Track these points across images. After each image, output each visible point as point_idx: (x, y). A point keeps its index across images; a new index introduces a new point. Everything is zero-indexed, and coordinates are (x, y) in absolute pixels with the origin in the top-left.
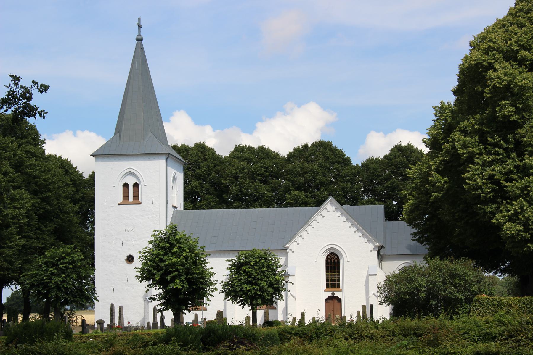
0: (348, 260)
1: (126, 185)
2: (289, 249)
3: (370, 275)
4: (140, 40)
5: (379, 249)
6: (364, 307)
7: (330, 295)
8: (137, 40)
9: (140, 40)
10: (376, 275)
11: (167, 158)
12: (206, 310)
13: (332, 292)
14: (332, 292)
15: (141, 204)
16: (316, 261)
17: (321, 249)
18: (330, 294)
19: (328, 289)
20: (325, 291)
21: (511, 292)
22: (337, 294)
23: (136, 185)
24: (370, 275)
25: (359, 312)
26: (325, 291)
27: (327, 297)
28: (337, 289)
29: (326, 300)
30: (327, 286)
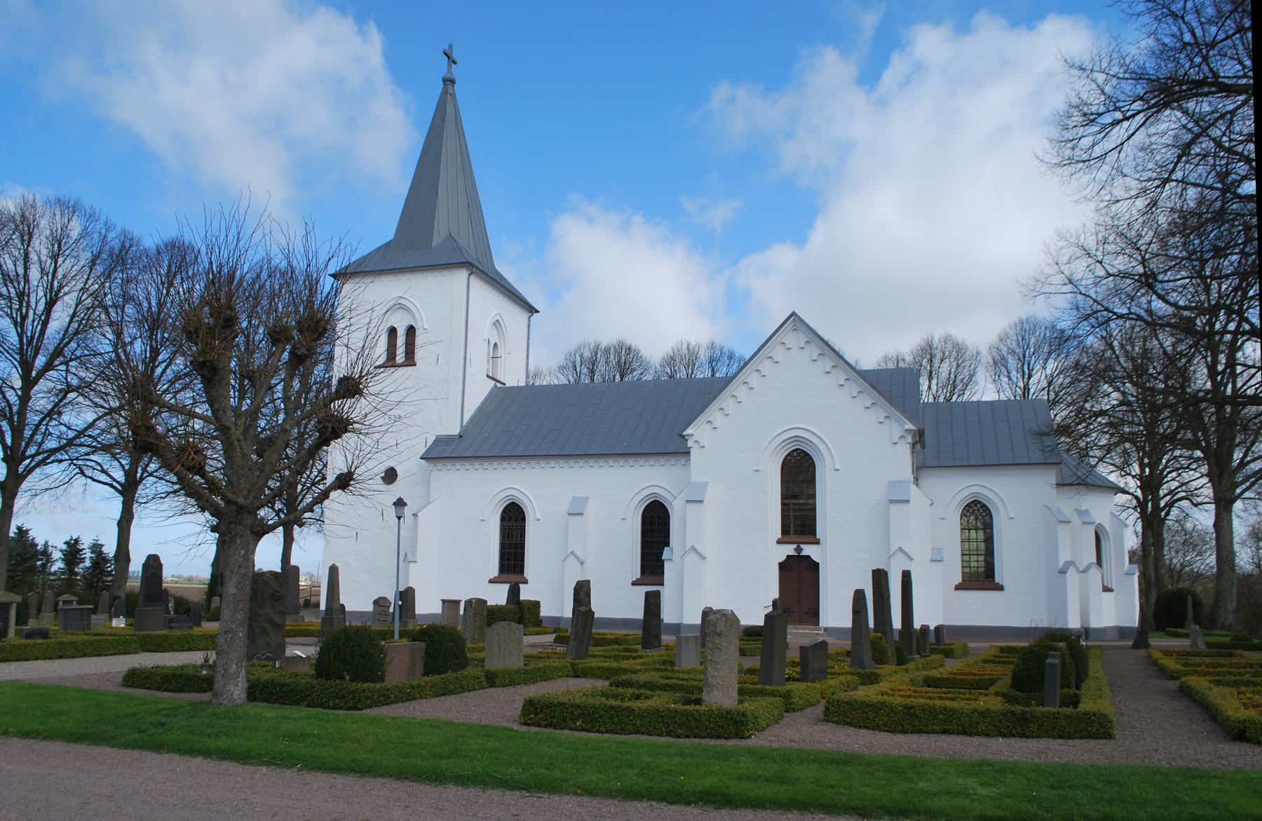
0: (838, 467)
1: (393, 332)
2: (694, 438)
3: (892, 501)
4: (449, 81)
5: (919, 439)
6: (880, 578)
7: (793, 553)
8: (445, 80)
9: (449, 81)
10: (582, 514)
11: (470, 275)
12: (527, 583)
13: (795, 546)
14: (795, 546)
15: (908, 501)
16: (756, 468)
17: (771, 439)
18: (789, 550)
19: (787, 538)
20: (779, 542)
21: (191, 440)
22: (808, 550)
23: (411, 331)
24: (892, 501)
25: (859, 596)
26: (779, 542)
27: (783, 558)
28: (810, 539)
29: (782, 565)
30: (785, 530)
